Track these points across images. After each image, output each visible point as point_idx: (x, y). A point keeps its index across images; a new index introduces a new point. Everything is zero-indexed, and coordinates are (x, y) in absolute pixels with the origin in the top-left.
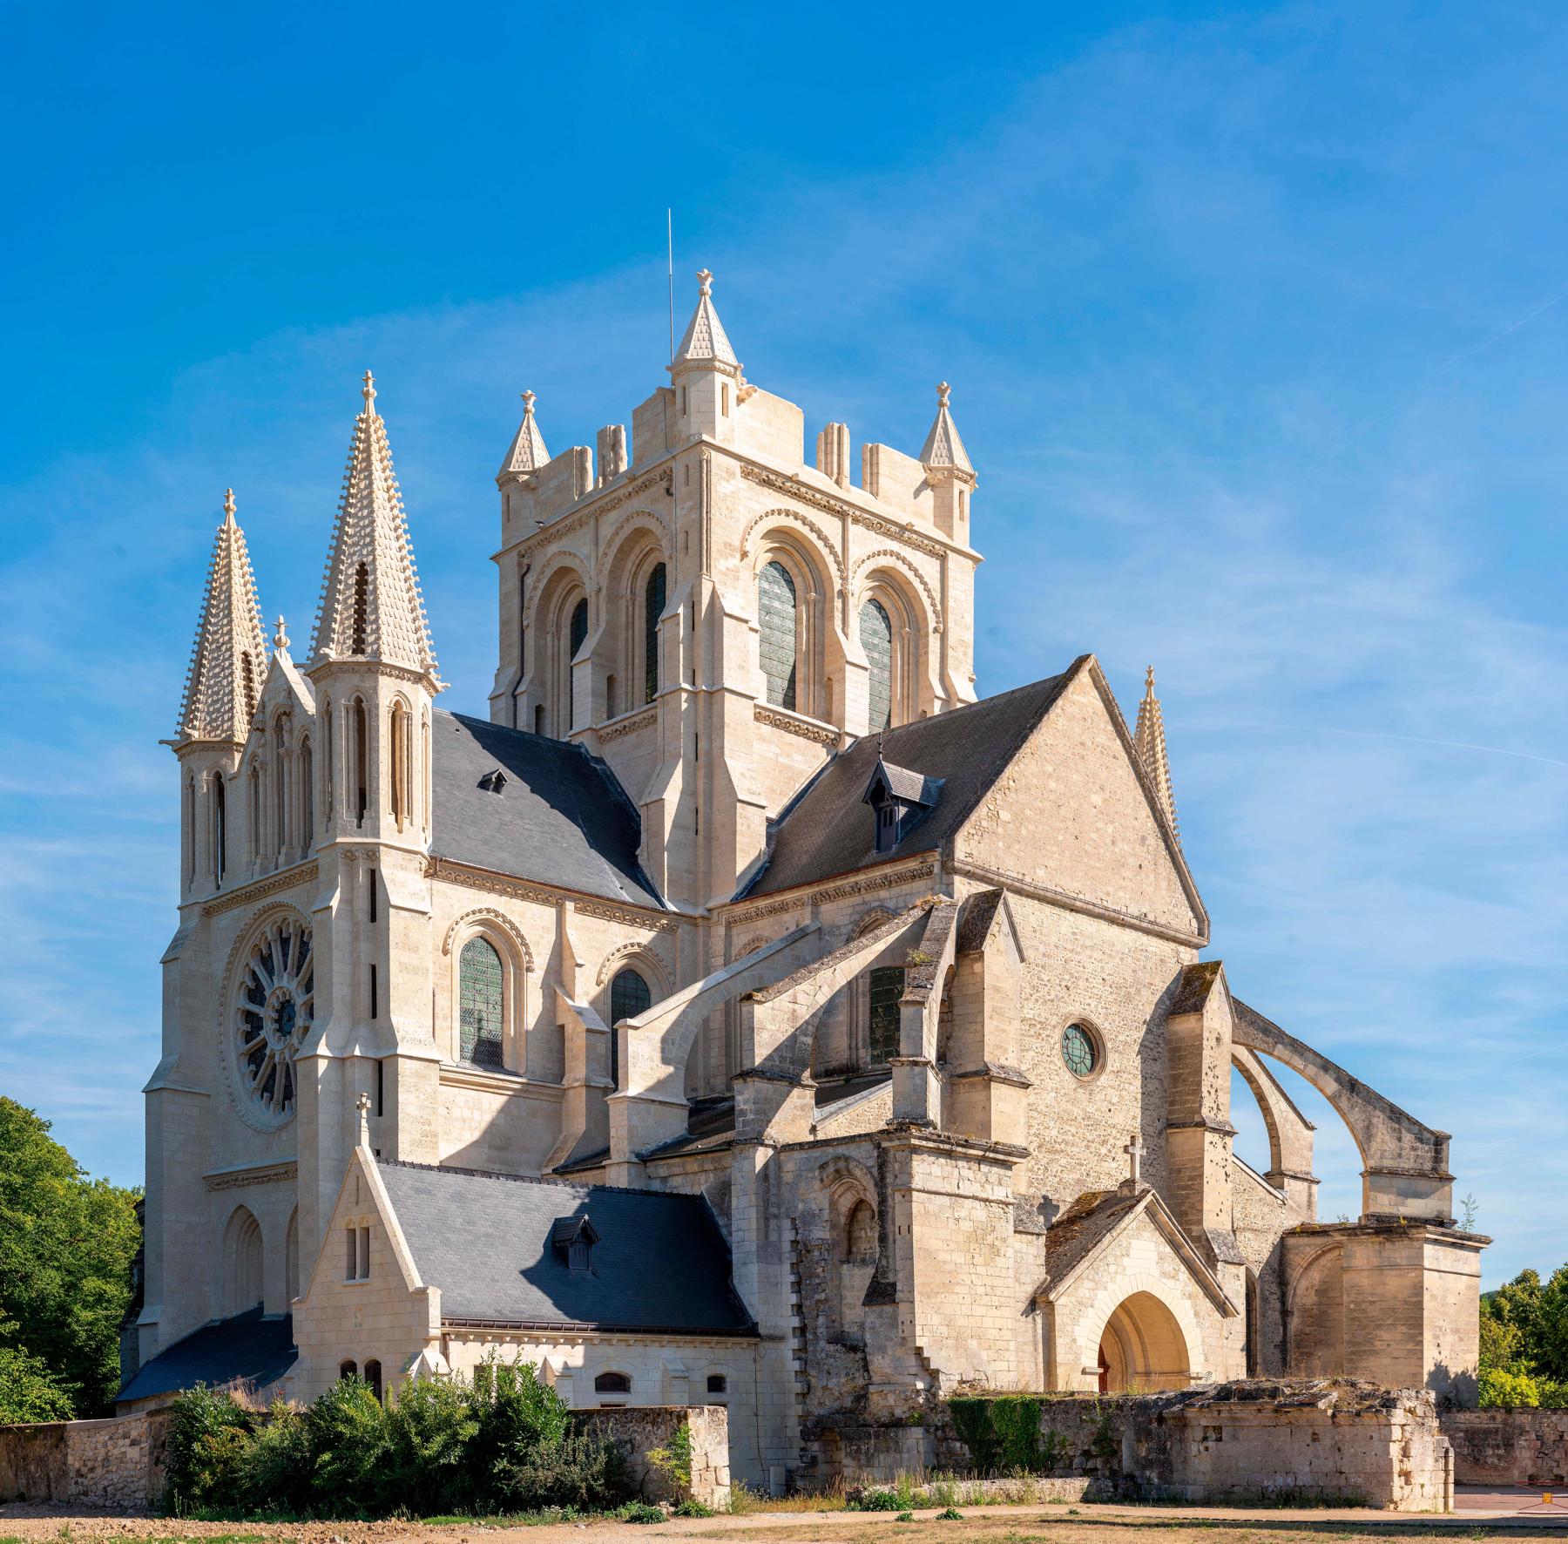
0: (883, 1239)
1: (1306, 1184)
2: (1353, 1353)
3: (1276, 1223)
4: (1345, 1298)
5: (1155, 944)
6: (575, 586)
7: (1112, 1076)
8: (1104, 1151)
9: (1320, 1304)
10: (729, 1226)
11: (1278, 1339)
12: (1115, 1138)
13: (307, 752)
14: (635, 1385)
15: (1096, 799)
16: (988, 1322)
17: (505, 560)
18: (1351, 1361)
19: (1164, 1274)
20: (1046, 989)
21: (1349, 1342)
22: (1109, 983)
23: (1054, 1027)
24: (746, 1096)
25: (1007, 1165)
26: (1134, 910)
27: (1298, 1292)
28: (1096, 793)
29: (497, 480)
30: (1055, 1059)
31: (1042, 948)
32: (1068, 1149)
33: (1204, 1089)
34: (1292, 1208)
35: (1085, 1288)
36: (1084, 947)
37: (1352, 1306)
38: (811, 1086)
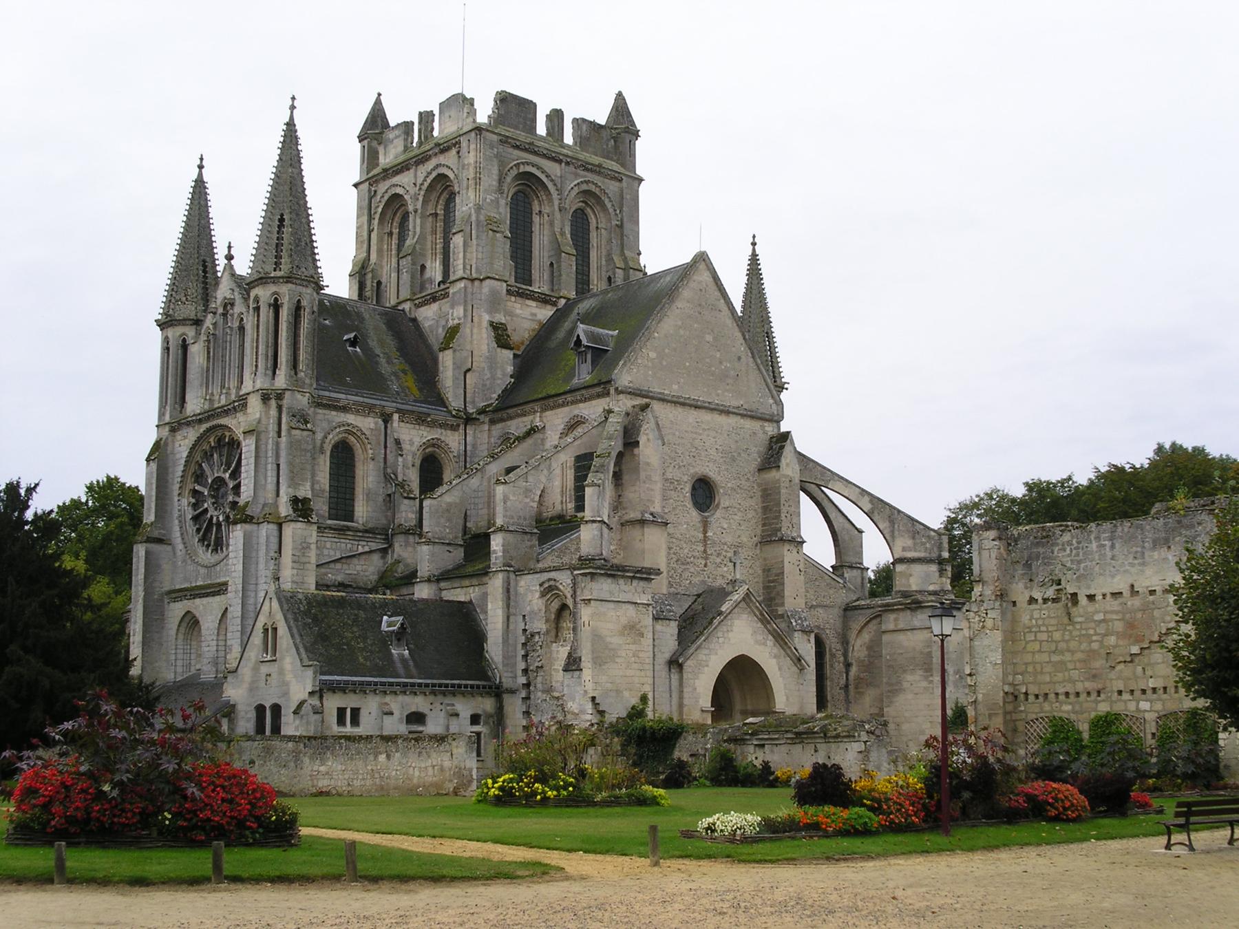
0: (575, 629)
1: (859, 571)
2: (889, 691)
3: (839, 601)
4: (884, 652)
5: (749, 424)
6: (403, 205)
7: (724, 511)
8: (718, 560)
9: (869, 656)
10: (486, 619)
11: (843, 682)
12: (726, 551)
13: (242, 329)
14: (429, 721)
15: (709, 338)
16: (636, 680)
17: (361, 187)
18: (888, 697)
19: (757, 642)
20: (681, 459)
21: (886, 683)
22: (721, 450)
23: (686, 482)
24: (497, 542)
25: (648, 580)
26: (735, 403)
27: (855, 649)
28: (709, 334)
29: (358, 137)
30: (687, 504)
31: (677, 433)
32: (696, 561)
33: (783, 515)
34: (850, 589)
35: (701, 655)
36: (704, 430)
37: (888, 657)
38: (536, 533)
